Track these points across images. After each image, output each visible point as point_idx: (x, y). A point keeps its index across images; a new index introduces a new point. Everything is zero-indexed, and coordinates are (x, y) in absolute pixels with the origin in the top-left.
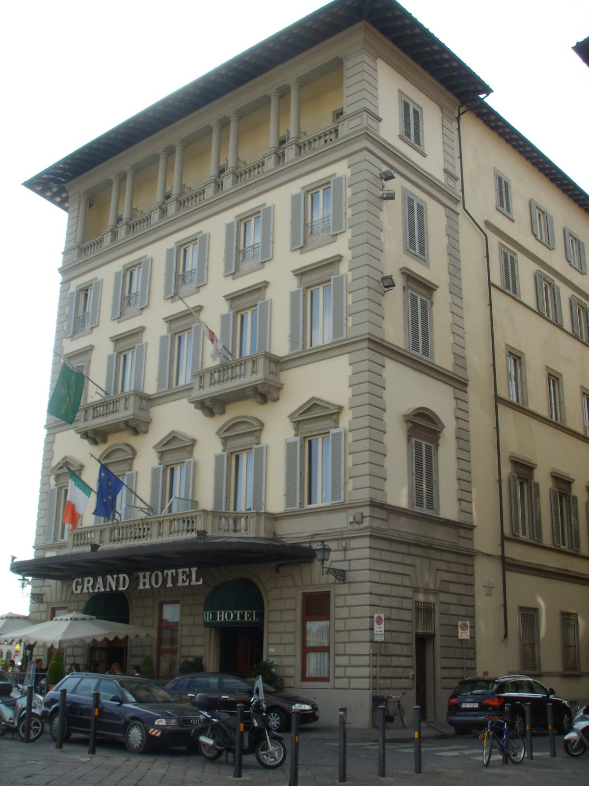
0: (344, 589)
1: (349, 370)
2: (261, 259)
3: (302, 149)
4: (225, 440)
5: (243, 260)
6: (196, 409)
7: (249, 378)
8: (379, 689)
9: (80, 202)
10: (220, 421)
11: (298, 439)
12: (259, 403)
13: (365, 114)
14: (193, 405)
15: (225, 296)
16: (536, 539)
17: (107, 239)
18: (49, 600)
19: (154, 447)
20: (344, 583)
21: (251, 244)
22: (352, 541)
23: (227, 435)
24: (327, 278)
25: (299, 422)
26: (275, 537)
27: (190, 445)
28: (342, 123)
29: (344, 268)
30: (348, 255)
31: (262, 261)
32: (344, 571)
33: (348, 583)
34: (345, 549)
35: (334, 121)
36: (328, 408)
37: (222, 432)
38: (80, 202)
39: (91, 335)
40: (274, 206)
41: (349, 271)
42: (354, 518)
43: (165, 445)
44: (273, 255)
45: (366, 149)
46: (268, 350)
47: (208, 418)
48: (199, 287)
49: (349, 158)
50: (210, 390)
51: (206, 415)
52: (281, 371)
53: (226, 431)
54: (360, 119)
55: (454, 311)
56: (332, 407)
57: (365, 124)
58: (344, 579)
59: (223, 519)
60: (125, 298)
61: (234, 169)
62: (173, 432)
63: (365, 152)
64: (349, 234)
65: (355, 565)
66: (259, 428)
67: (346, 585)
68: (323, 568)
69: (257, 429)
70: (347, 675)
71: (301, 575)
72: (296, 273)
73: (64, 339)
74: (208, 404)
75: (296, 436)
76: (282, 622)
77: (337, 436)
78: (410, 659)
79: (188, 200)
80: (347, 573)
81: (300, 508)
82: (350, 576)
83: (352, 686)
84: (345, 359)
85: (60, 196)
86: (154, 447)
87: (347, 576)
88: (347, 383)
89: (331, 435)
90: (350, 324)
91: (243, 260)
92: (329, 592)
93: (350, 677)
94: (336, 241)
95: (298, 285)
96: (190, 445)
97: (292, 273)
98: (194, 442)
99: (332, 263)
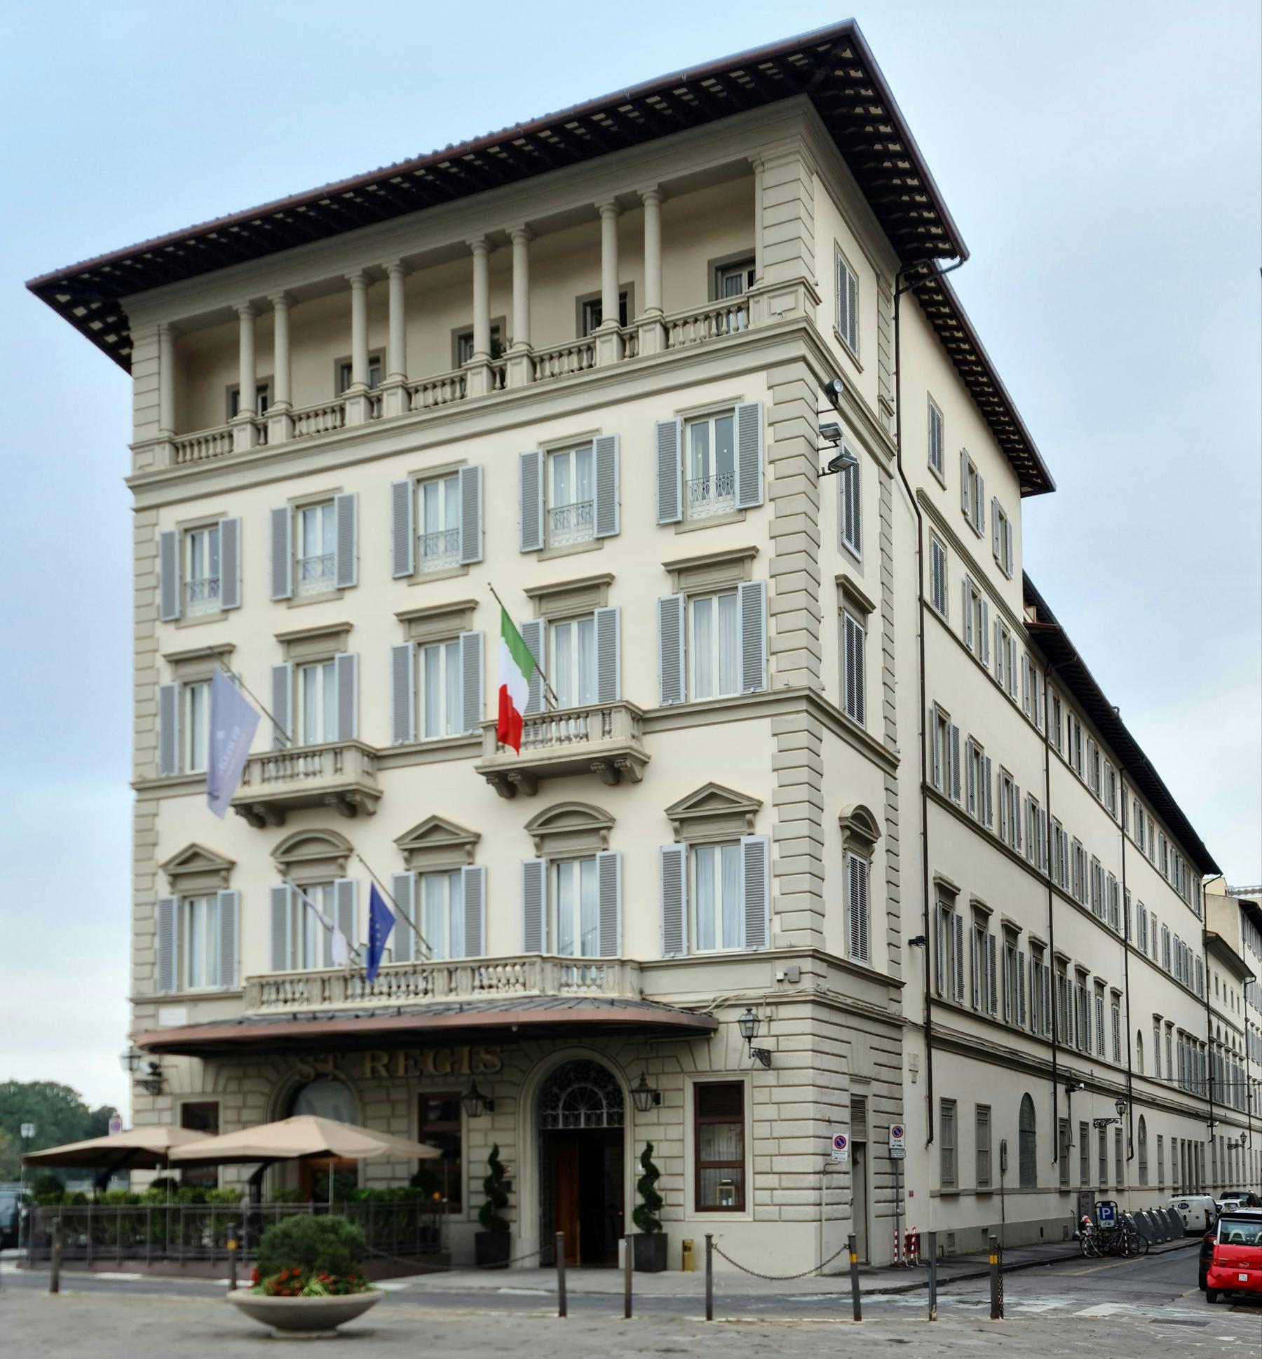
0: (770, 1077)
1: (772, 745)
2: (464, 559)
3: (538, 367)
4: (287, 867)
5: (304, 578)
6: (488, 783)
7: (325, 779)
8: (826, 1220)
9: (159, 342)
10: (532, 808)
11: (175, 897)
12: (342, 814)
13: (802, 289)
14: (484, 778)
15: (277, 636)
16: (1019, 1024)
17: (243, 439)
18: (177, 1090)
19: (395, 841)
20: (770, 1069)
21: (319, 553)
22: (779, 1007)
23: (288, 860)
24: (587, 610)
25: (682, 821)
26: (645, 1002)
27: (468, 844)
28: (756, 299)
29: (759, 572)
30: (768, 550)
31: (742, 507)
32: (769, 1052)
33: (774, 1069)
34: (771, 1020)
35: (337, 396)
36: (457, 834)
37: (535, 826)
38: (159, 342)
39: (337, 603)
40: (358, 494)
41: (772, 577)
42: (786, 974)
43: (416, 838)
44: (620, 529)
45: (804, 359)
46: (355, 737)
47: (503, 799)
48: (468, 565)
49: (769, 370)
50: (260, 789)
51: (501, 795)
52: (380, 770)
53: (545, 823)
54: (792, 296)
55: (887, 682)
56: (463, 834)
57: (799, 313)
58: (769, 1065)
59: (575, 969)
60: (419, 538)
61: (367, 388)
62: (193, 845)
63: (802, 365)
64: (769, 512)
65: (785, 1044)
66: (345, 853)
67: (771, 1072)
68: (750, 1048)
69: (600, 828)
70: (776, 1201)
71: (694, 1059)
72: (670, 568)
73: (158, 624)
74: (257, 810)
75: (172, 893)
76: (659, 1124)
77: (755, 852)
78: (847, 1176)
79: (215, 439)
80: (772, 1054)
81: (688, 954)
82: (778, 1059)
83: (784, 1217)
84: (762, 728)
85: (102, 319)
86: (395, 841)
87: (772, 1059)
88: (769, 766)
89: (742, 847)
90: (773, 669)
91: (192, 600)
92: (743, 1081)
93: (780, 1205)
94: (602, 548)
95: (405, 636)
96: (468, 844)
97: (525, 594)
98: (232, 865)
99: (596, 587)
